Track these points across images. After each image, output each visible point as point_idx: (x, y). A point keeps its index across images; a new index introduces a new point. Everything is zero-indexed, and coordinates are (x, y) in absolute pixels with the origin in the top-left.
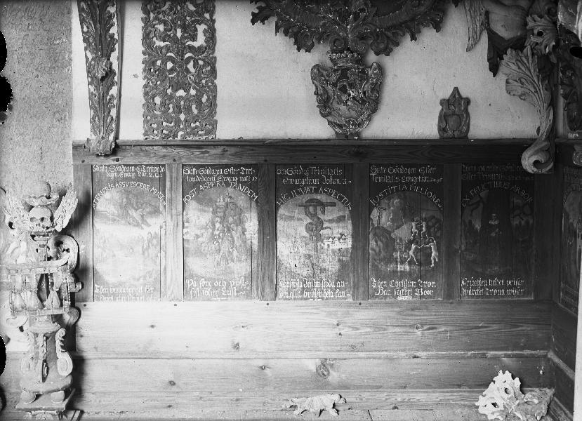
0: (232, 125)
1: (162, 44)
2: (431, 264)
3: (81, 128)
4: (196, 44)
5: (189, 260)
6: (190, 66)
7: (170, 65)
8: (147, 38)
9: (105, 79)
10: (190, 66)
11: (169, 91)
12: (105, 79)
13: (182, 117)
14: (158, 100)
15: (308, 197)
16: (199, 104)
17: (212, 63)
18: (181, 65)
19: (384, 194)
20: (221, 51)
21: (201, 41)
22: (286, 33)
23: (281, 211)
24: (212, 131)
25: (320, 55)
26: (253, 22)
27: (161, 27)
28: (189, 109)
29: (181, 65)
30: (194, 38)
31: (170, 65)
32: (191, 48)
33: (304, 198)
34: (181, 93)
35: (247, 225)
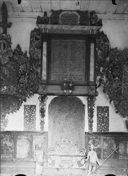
0: (111, 129)
1: (100, 116)
2: (77, 16)
3: (87, 129)
4: (106, 116)
5: (104, 152)
6: (105, 120)
7: (101, 120)
8: (98, 115)
9: (91, 122)
10: (105, 120)
11: (101, 124)
12: (91, 122)
13: (103, 128)
14: (99, 125)
15: (124, 142)
16: (106, 126)
17: (108, 119)
18: (103, 120)
19: (3, 116)
20: (109, 117)
21: (106, 116)
22: (121, 115)
23: (120, 144)
24: (108, 131)
25: (126, 119)
26: (116, 113)
27: (100, 113)
28: (104, 127)
29: (103, 120)
30: (105, 115)
31: (101, 120)
32: (105, 117)
33: (124, 142)
34: (103, 124)
35: (4, 167)
